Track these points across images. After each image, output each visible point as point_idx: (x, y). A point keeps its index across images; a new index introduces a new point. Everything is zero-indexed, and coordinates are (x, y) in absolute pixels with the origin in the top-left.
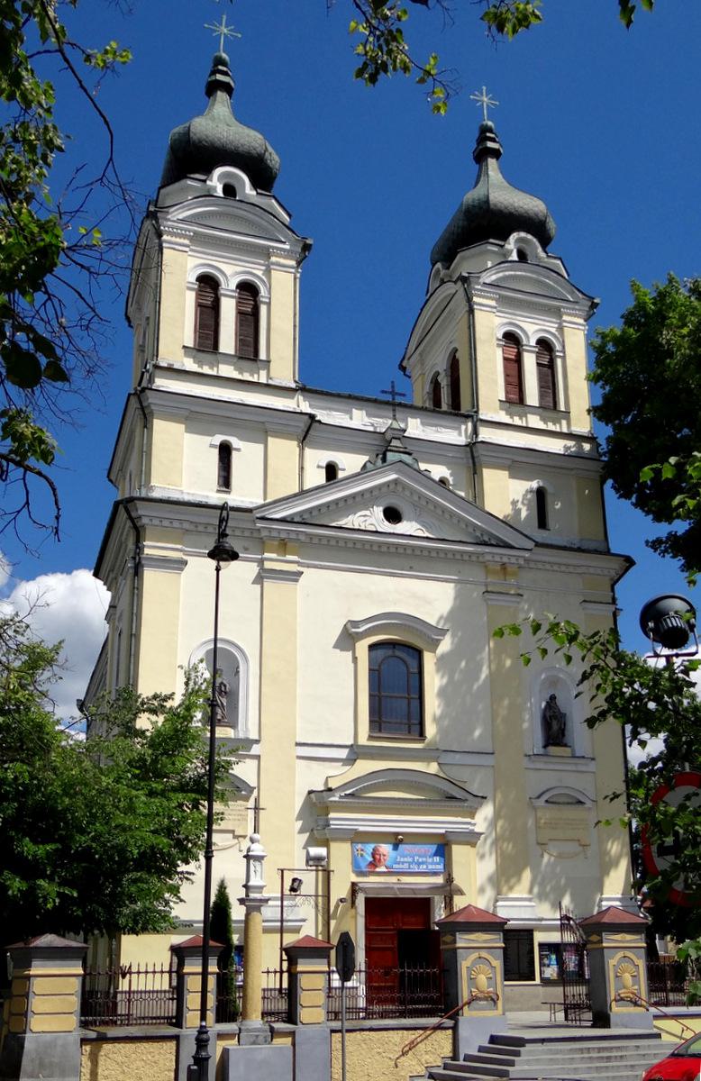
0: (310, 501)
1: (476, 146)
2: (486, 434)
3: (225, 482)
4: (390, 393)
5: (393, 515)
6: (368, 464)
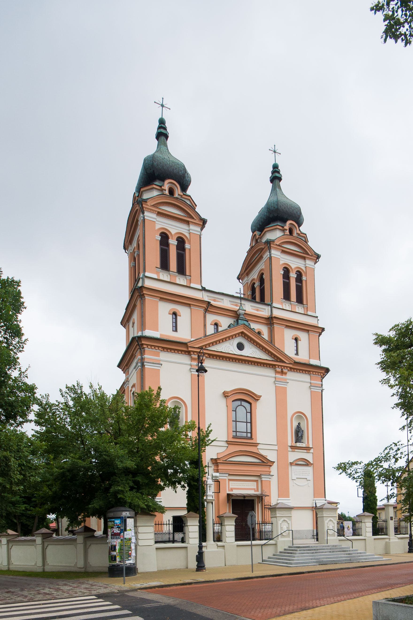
0: (304, 367)
1: (271, 175)
2: (276, 313)
3: (297, 354)
4: (239, 293)
5: (240, 347)
6: (231, 325)
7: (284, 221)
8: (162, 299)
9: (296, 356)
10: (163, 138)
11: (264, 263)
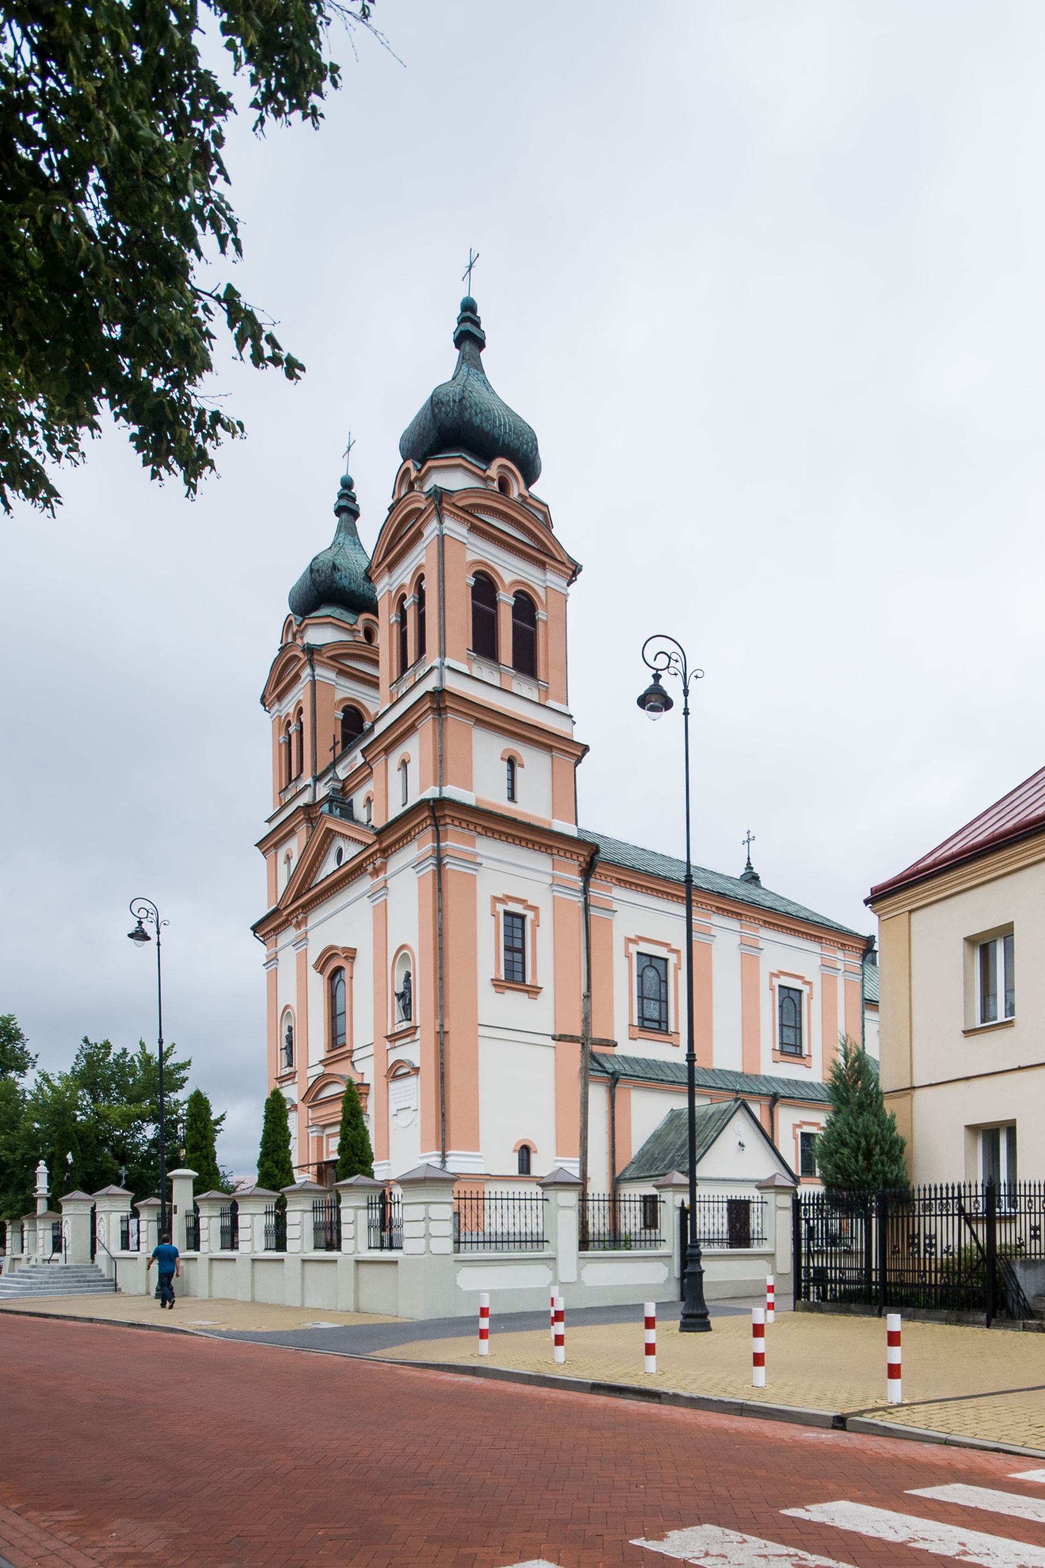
3: (512, 798)
7: (487, 458)
8: (479, 722)
9: (511, 805)
10: (467, 346)
11: (424, 552)
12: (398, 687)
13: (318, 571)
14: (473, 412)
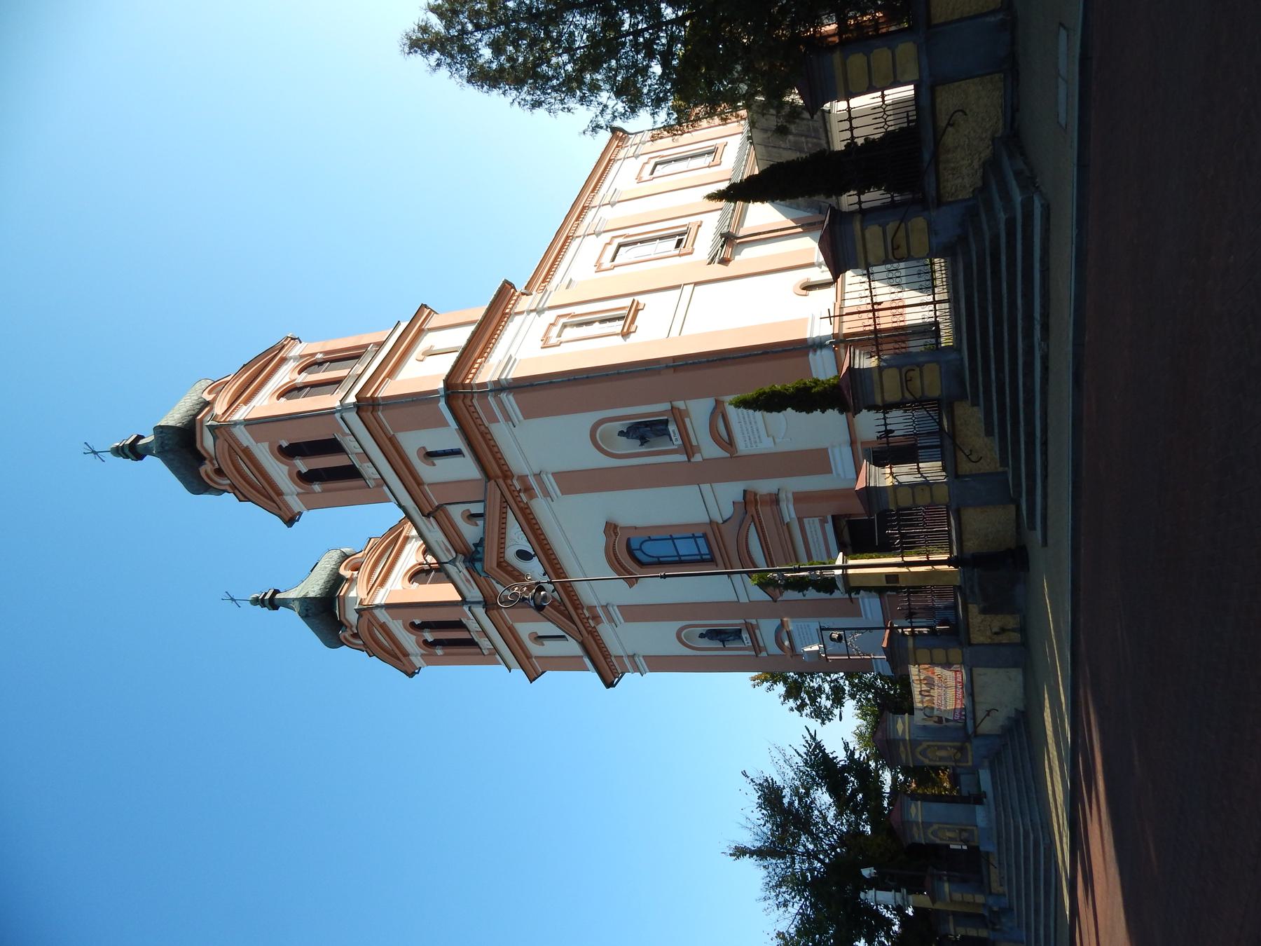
12: (370, 478)
13: (307, 610)
14: (171, 419)
